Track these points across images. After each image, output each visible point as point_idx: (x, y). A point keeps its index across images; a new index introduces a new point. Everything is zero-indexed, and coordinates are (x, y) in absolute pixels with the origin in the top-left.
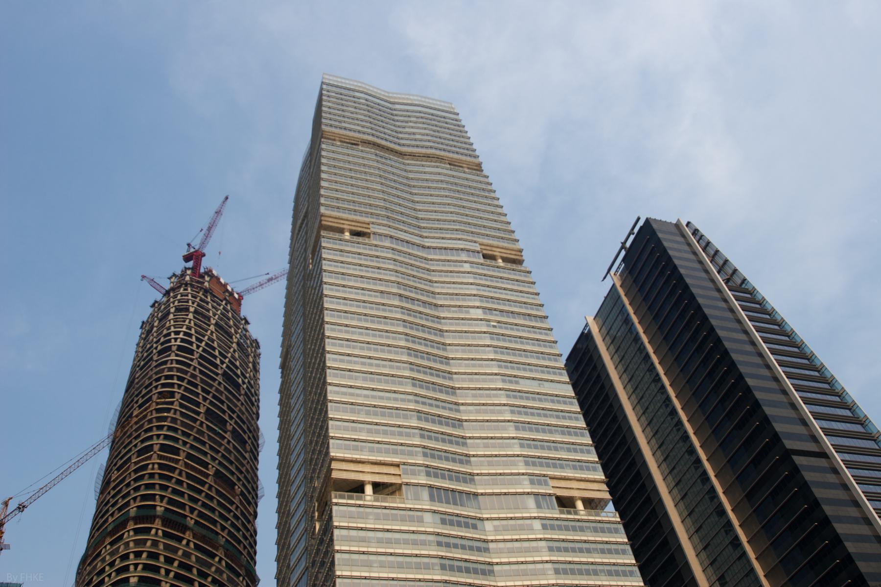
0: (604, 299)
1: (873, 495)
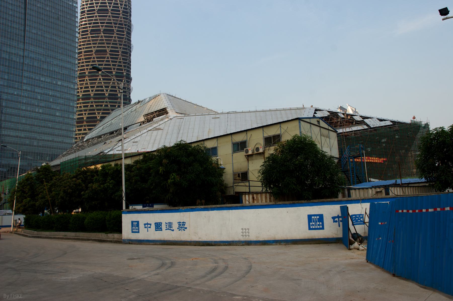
0: (380, 185)
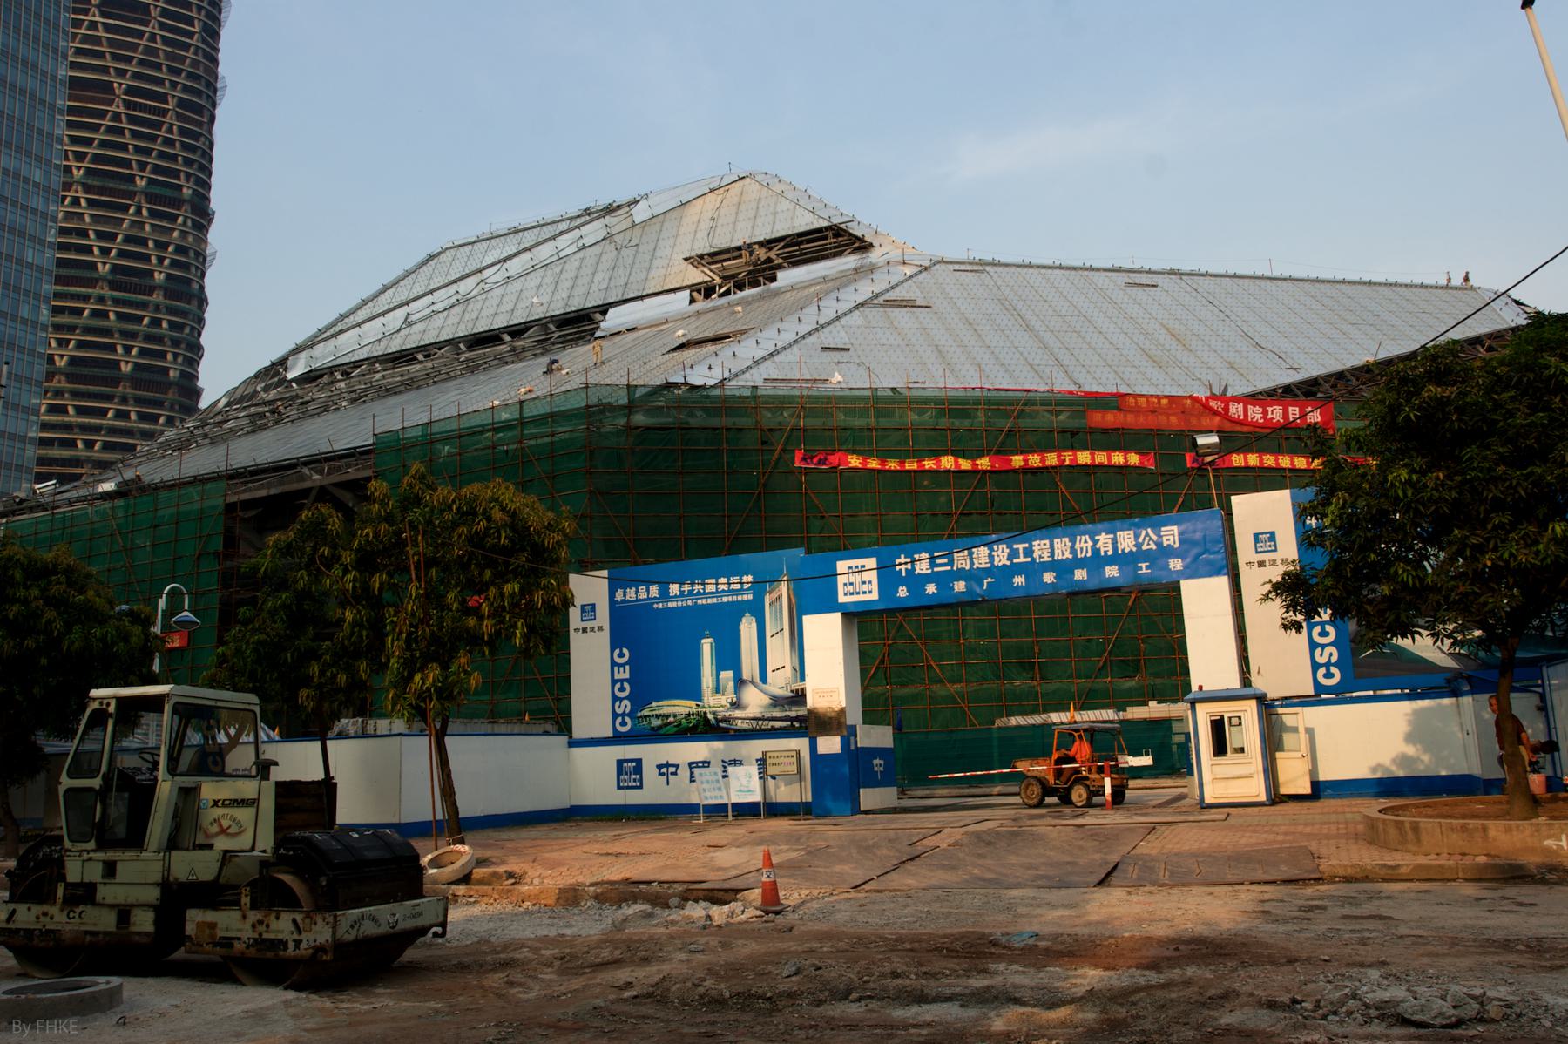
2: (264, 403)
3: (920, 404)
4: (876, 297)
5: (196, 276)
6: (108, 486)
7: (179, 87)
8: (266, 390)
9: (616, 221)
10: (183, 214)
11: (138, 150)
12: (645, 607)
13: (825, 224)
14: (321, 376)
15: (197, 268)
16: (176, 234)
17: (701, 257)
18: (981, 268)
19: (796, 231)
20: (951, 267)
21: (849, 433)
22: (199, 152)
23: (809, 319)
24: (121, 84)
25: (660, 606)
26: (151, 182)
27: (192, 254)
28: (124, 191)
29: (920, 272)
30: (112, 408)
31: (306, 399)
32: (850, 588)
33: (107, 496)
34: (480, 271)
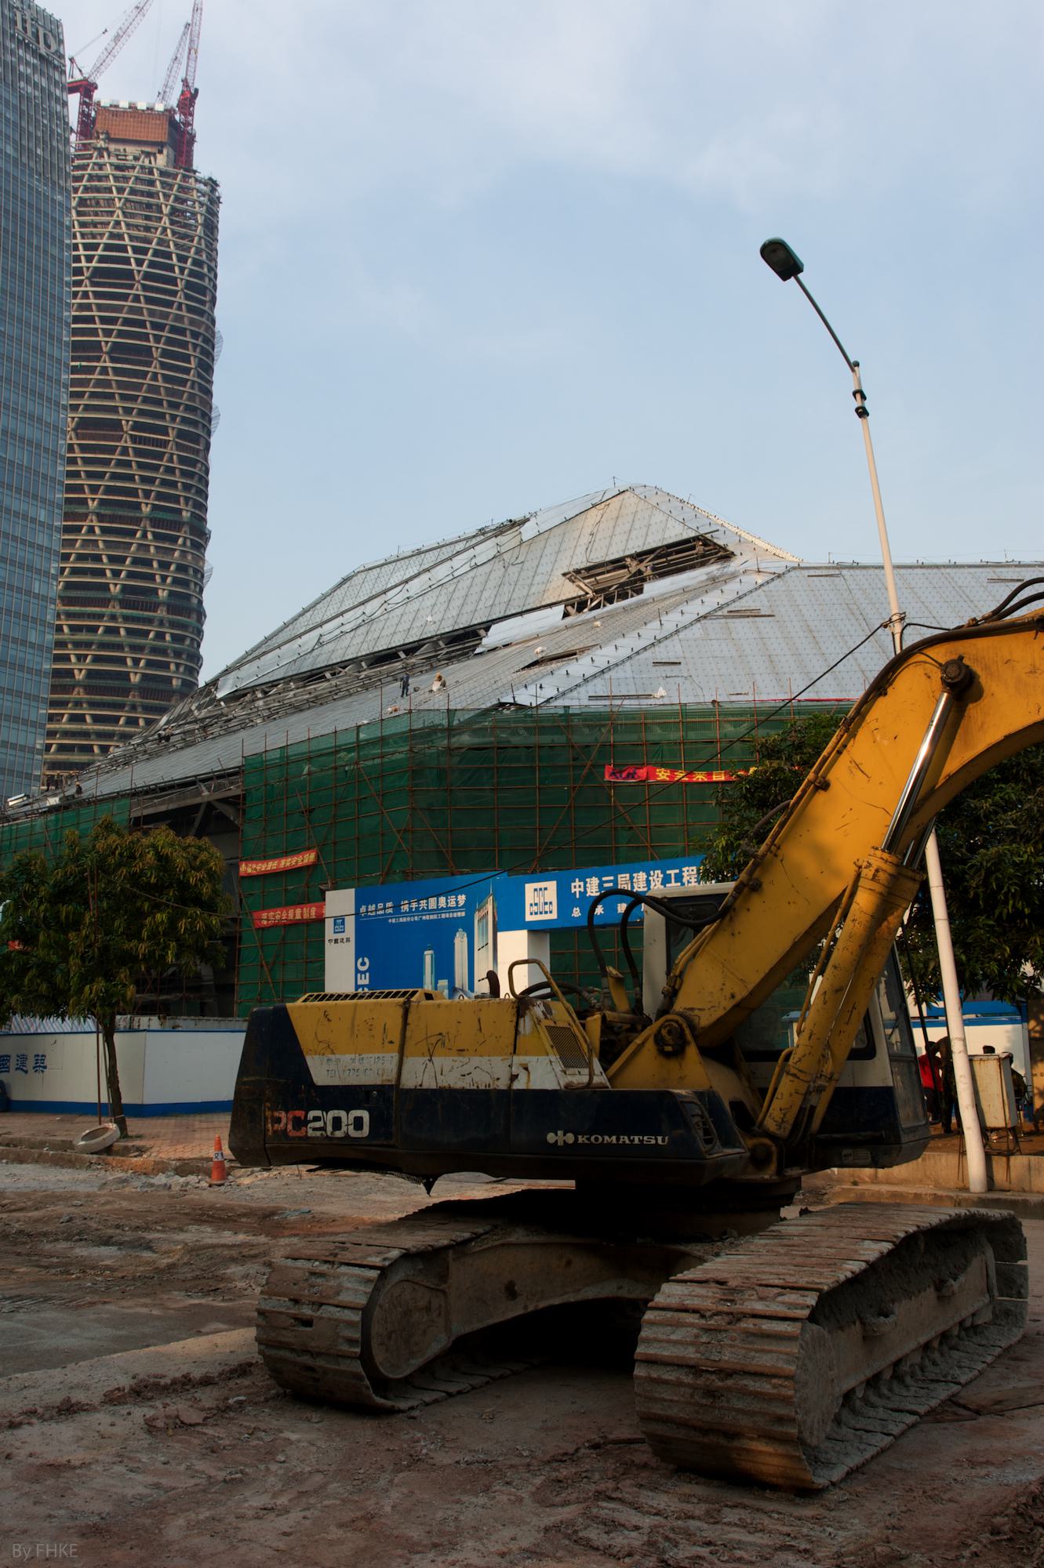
1: (110, 683)
2: (196, 721)
3: (737, 715)
4: (721, 608)
5: (195, 591)
6: (53, 801)
7: (178, 419)
8: (199, 708)
9: (508, 540)
10: (183, 534)
11: (144, 480)
12: (383, 921)
13: (692, 534)
14: (245, 695)
15: (196, 584)
16: (177, 554)
17: (578, 572)
18: (837, 572)
19: (665, 543)
20: (806, 573)
21: (658, 747)
22: (196, 478)
23: (651, 631)
24: (128, 421)
25: (394, 921)
26: (155, 508)
27: (191, 572)
28: (132, 518)
29: (773, 579)
30: (123, 716)
31: (230, 716)
32: (535, 908)
33: (53, 809)
34: (385, 592)
